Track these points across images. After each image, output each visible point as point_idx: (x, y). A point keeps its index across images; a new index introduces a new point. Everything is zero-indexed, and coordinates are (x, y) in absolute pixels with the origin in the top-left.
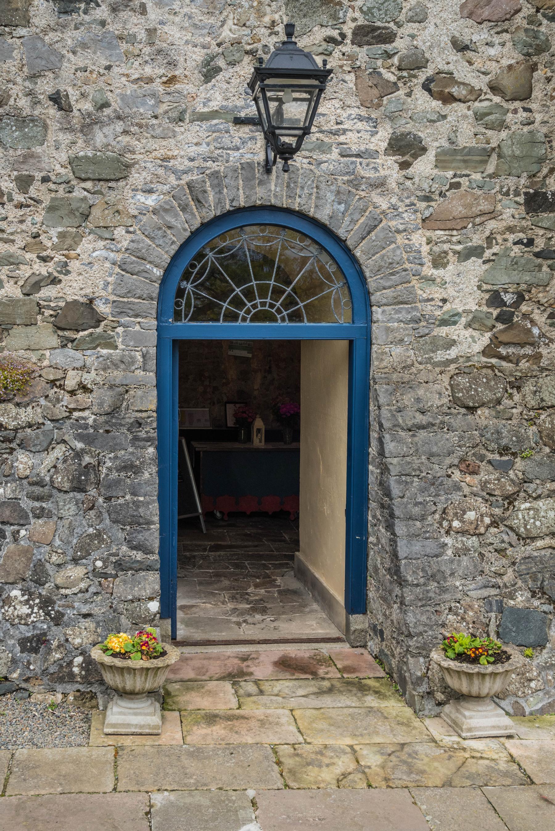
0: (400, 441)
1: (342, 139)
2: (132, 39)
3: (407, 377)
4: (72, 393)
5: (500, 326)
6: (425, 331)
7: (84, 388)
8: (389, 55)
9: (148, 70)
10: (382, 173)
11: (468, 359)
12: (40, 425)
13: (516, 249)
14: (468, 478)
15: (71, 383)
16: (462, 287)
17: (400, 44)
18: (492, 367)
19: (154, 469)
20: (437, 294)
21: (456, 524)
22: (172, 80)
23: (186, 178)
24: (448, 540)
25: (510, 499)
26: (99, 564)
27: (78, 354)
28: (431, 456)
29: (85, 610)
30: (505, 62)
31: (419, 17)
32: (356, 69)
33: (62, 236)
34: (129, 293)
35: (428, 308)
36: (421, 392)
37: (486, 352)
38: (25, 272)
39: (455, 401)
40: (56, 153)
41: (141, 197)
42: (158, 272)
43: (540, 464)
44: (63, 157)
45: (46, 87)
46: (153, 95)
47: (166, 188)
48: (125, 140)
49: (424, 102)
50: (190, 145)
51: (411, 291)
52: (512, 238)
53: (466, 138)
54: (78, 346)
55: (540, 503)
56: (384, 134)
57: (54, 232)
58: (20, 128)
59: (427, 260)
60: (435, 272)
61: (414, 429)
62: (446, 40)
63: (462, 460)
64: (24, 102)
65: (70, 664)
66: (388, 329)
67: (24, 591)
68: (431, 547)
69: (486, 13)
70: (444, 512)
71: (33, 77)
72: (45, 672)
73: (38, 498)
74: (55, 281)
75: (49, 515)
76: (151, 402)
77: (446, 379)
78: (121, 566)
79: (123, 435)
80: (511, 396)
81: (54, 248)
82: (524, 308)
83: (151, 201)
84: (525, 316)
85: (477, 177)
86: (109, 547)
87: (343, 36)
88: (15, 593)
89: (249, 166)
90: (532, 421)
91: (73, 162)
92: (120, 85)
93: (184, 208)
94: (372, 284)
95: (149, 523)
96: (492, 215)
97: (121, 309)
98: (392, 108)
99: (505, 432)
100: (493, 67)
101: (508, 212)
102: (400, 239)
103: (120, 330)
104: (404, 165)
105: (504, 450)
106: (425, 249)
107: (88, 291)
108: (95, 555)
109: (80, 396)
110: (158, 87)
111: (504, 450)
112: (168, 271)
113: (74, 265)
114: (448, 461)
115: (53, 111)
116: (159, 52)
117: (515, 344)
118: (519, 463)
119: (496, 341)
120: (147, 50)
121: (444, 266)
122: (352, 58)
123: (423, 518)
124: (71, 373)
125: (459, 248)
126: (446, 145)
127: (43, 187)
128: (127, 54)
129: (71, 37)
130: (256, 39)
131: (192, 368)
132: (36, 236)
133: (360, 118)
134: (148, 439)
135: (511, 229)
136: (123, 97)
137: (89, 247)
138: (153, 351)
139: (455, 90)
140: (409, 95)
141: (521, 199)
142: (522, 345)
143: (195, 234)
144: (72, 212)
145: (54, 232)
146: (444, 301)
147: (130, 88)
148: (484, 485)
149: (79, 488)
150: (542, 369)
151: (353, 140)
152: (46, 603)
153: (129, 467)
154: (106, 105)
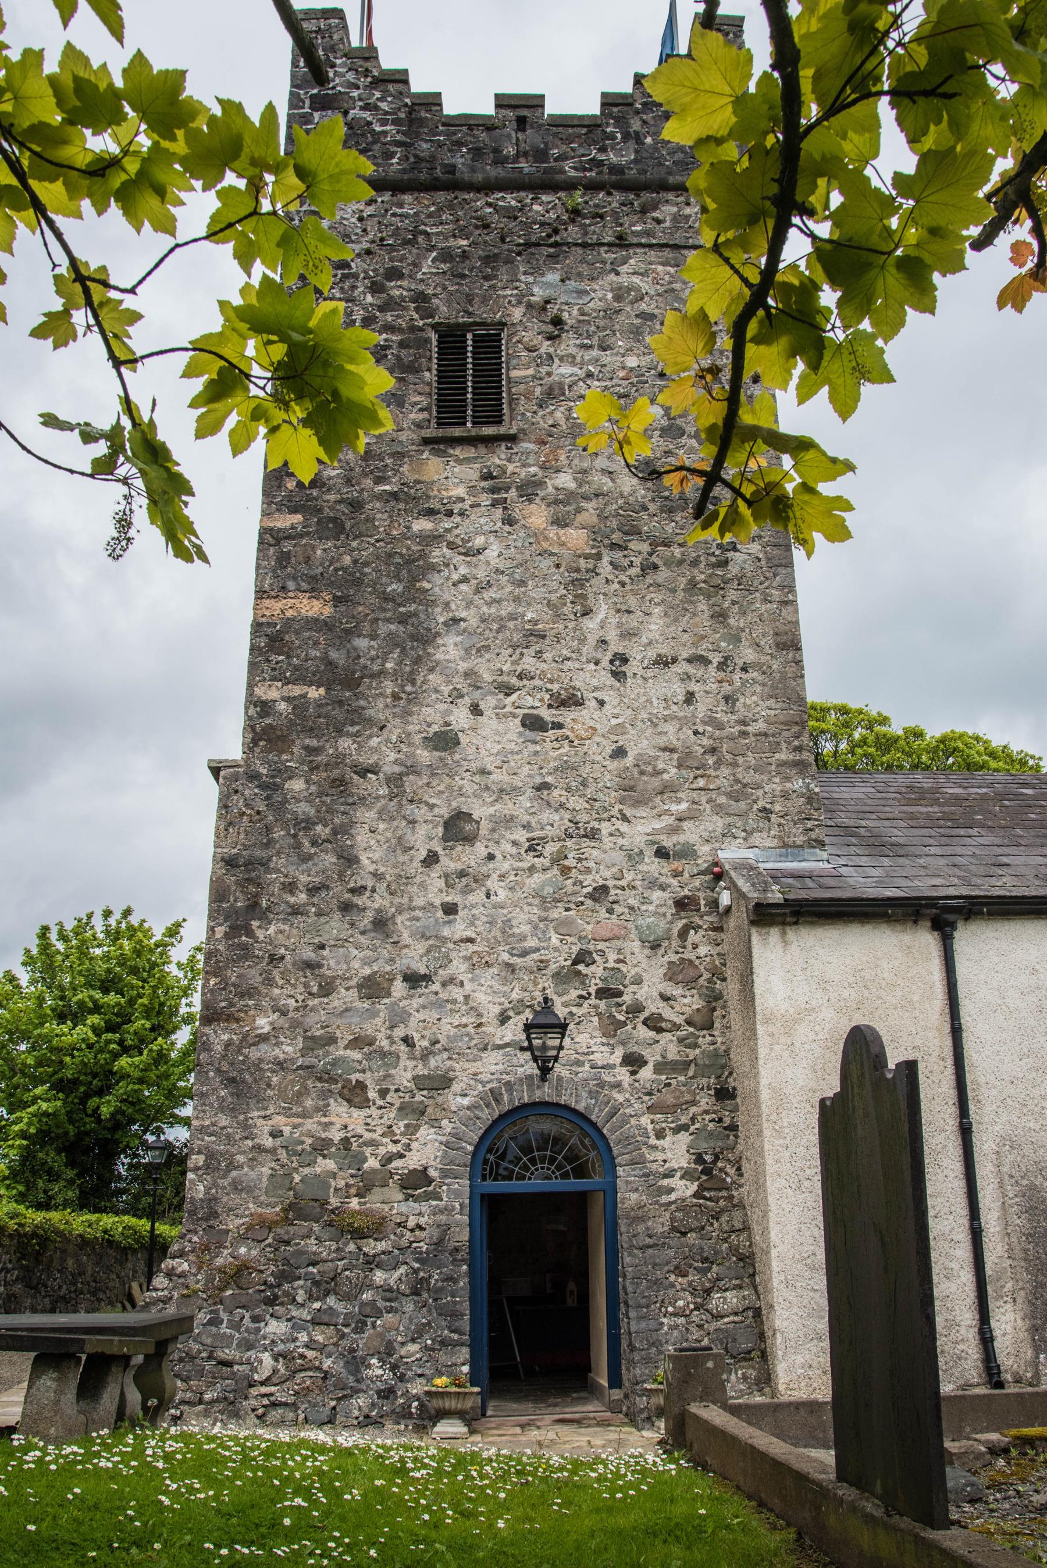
0: (634, 1256)
1: (591, 1057)
2: (454, 1002)
3: (640, 1214)
4: (412, 1230)
5: (704, 1178)
6: (654, 1183)
7: (421, 1228)
8: (619, 1005)
9: (464, 1020)
10: (619, 1078)
11: (684, 1200)
12: (390, 1253)
13: (711, 1125)
14: (680, 1279)
15: (411, 1224)
16: (676, 1151)
17: (627, 998)
18: (700, 1206)
19: (467, 1280)
20: (660, 1156)
21: (670, 1309)
22: (480, 1025)
23: (489, 1086)
24: (665, 1320)
25: (708, 1292)
26: (429, 1342)
27: (416, 1205)
28: (655, 1265)
29: (419, 1372)
30: (695, 1007)
31: (638, 981)
32: (599, 1014)
33: (407, 1126)
34: (451, 1163)
35: (654, 1167)
36: (650, 1223)
37: (695, 1195)
38: (382, 1151)
39: (673, 1229)
40: (405, 1073)
41: (459, 1099)
42: (470, 1148)
43: (729, 1268)
44: (409, 1075)
45: (399, 1032)
46: (468, 1035)
47: (476, 1093)
48: (449, 1063)
49: (644, 1033)
50: (491, 1065)
51: (642, 1155)
52: (707, 1117)
53: (673, 1054)
54: (417, 1199)
55: (728, 1294)
56: (619, 1053)
57: (402, 1124)
58: (382, 1059)
59: (652, 1134)
60: (658, 1142)
61: (644, 1248)
62: (655, 994)
63: (677, 1267)
64: (385, 1043)
65: (410, 1406)
66: (627, 1182)
67: (380, 1360)
68: (652, 1324)
69: (680, 978)
70: (663, 1301)
71: (391, 1028)
72: (393, 1411)
73: (389, 1300)
74: (402, 1156)
75: (396, 1312)
76: (465, 1236)
77: (668, 1215)
78: (444, 1343)
79: (446, 1257)
80: (712, 1224)
81: (402, 1134)
82: (720, 1164)
83: (466, 1101)
84: (721, 1170)
85: (682, 1078)
86: (435, 1331)
87: (589, 994)
88: (374, 1361)
89: (530, 1077)
90: (725, 1240)
91: (416, 1078)
92: (446, 1029)
93: (488, 1106)
94: (615, 1152)
95: (463, 1315)
96: (694, 1103)
97: (445, 1174)
98: (623, 1037)
99: (706, 1248)
100: (687, 1009)
101: (704, 1101)
102: (633, 1121)
103: (445, 1188)
104: (633, 1073)
105: (705, 1260)
106: (650, 1127)
107: (424, 1162)
108: (426, 1336)
109: (417, 1233)
110: (471, 1029)
111: (705, 1260)
112: (477, 1147)
113: (415, 1145)
114: (666, 1268)
115: (403, 1048)
116: (472, 1008)
117: (715, 1189)
118: (715, 1268)
119: (702, 1188)
120: (464, 1008)
121: (664, 1138)
122: (596, 1007)
123: (648, 1306)
124: (411, 1218)
125: (673, 1125)
126: (660, 1059)
127: (395, 1095)
128: (451, 1010)
129: (416, 1002)
130: (533, 998)
131: (494, 1212)
132: (390, 1127)
133: (603, 1044)
134: (463, 1260)
135: (706, 1112)
136: (448, 1037)
137: (425, 1133)
138: (467, 1201)
139: (663, 1025)
140: (634, 1028)
141: (712, 1092)
142: (720, 1190)
143: (495, 1122)
144: (414, 1110)
145: (402, 1124)
146: (665, 1161)
147: (453, 1031)
148: (690, 1284)
149: (416, 1292)
150: (734, 1206)
151: (599, 1058)
152: (394, 1368)
153: (449, 1279)
154: (438, 1042)
